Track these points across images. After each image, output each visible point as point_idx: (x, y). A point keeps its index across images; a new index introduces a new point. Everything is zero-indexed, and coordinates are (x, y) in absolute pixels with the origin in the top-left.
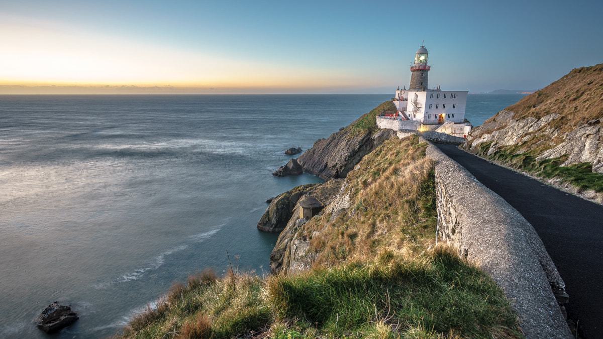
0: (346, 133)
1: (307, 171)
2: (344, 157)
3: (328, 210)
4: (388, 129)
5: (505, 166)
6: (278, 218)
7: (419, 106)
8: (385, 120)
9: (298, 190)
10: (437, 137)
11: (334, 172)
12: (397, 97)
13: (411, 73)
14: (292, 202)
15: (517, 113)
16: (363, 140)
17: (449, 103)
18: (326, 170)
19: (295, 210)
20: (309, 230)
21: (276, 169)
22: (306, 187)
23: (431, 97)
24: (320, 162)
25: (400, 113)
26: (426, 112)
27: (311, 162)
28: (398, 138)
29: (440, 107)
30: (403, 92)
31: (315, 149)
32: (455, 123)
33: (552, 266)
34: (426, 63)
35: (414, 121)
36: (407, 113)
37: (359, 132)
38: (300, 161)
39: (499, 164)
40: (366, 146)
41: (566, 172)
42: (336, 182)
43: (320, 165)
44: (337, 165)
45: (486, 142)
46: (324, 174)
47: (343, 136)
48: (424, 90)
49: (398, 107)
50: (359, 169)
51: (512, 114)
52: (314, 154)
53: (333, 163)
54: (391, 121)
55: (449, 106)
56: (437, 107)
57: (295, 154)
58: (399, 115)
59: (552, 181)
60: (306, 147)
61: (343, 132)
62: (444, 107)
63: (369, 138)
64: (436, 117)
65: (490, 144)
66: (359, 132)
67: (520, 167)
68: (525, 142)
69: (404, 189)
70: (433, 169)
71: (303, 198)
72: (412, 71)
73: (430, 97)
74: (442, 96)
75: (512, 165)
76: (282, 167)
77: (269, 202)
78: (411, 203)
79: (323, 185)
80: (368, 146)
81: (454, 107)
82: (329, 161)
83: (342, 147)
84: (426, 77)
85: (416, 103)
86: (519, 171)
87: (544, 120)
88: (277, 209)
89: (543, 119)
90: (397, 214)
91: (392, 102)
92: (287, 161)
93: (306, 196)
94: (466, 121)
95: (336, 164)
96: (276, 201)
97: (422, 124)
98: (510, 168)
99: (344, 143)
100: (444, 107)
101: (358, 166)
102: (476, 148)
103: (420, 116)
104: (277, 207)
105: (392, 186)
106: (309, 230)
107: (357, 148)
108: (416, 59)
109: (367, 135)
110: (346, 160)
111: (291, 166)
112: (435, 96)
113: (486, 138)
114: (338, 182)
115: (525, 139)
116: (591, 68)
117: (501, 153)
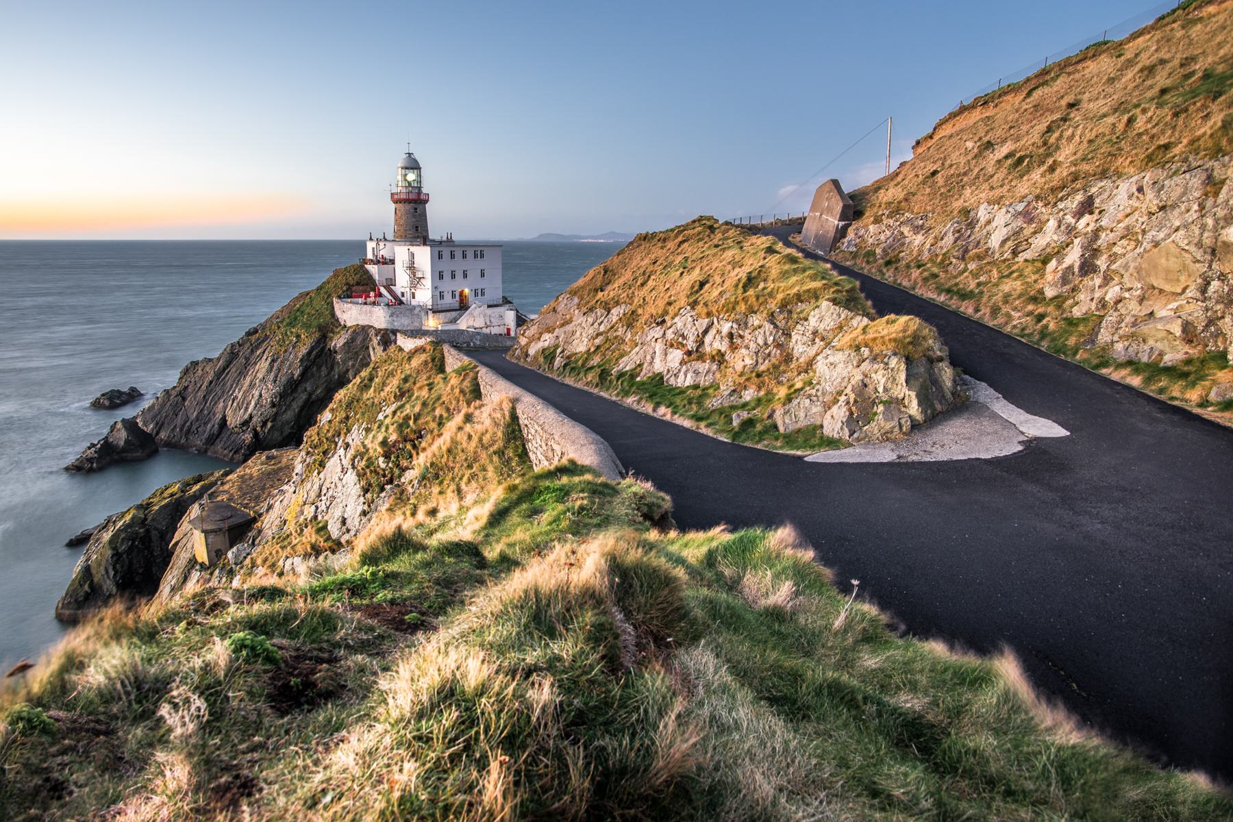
0: (263, 341)
1: (171, 445)
2: (267, 398)
3: (269, 523)
4: (363, 327)
5: (579, 385)
6: (122, 578)
7: (419, 275)
8: (353, 307)
9: (165, 495)
10: (467, 339)
11: (248, 437)
12: (370, 256)
13: (393, 206)
14: (156, 529)
15: (582, 299)
16: (309, 353)
17: (474, 266)
18: (225, 435)
19: (177, 543)
20: (268, 563)
21: (71, 460)
22: (188, 485)
23: (440, 257)
24: (203, 419)
25: (383, 290)
26: (435, 288)
27: (179, 421)
28: (401, 349)
29: (459, 275)
30: (382, 244)
31: (186, 388)
32: (489, 306)
33: (618, 462)
34: (420, 188)
35: (414, 307)
36: (398, 289)
37: (298, 336)
38: (145, 424)
39: (571, 383)
40: (319, 368)
41: (642, 387)
42: (268, 458)
43: (206, 424)
44: (254, 420)
45: (548, 348)
46: (219, 447)
47: (257, 348)
48: (425, 244)
49: (376, 277)
50: (330, 422)
51: (576, 300)
52: (184, 399)
53: (242, 416)
54: (368, 307)
55: (474, 275)
56: (453, 276)
57: (124, 404)
58: (380, 295)
59: (630, 401)
60: (156, 383)
61: (255, 339)
62: (465, 276)
63: (324, 348)
64: (453, 296)
65: (555, 350)
66: (298, 336)
67: (597, 385)
68: (598, 347)
69: (486, 439)
70: (513, 409)
71: (195, 511)
72: (396, 202)
73: (438, 257)
74: (458, 254)
75: (587, 384)
76: (93, 445)
77: (79, 542)
78: (500, 453)
79: (240, 471)
80: (323, 368)
81: (483, 275)
82: (229, 412)
83: (260, 376)
84: (424, 215)
85: (412, 268)
86: (596, 391)
87: (616, 313)
88: (117, 555)
89: (613, 311)
90: (484, 470)
91: (362, 267)
92: (98, 427)
93: (201, 505)
94: (506, 301)
95: (251, 417)
96: (107, 536)
97: (430, 314)
98: (586, 388)
99: (263, 365)
100: (465, 276)
101: (326, 416)
102: (535, 357)
103: (424, 296)
104: (115, 549)
105: (470, 437)
106: (268, 563)
107: (297, 373)
108: (399, 178)
109: (318, 342)
110: (273, 405)
111: (122, 436)
112: (445, 249)
113: (547, 340)
114: (273, 457)
115: (597, 341)
116: (654, 235)
117: (571, 365)
